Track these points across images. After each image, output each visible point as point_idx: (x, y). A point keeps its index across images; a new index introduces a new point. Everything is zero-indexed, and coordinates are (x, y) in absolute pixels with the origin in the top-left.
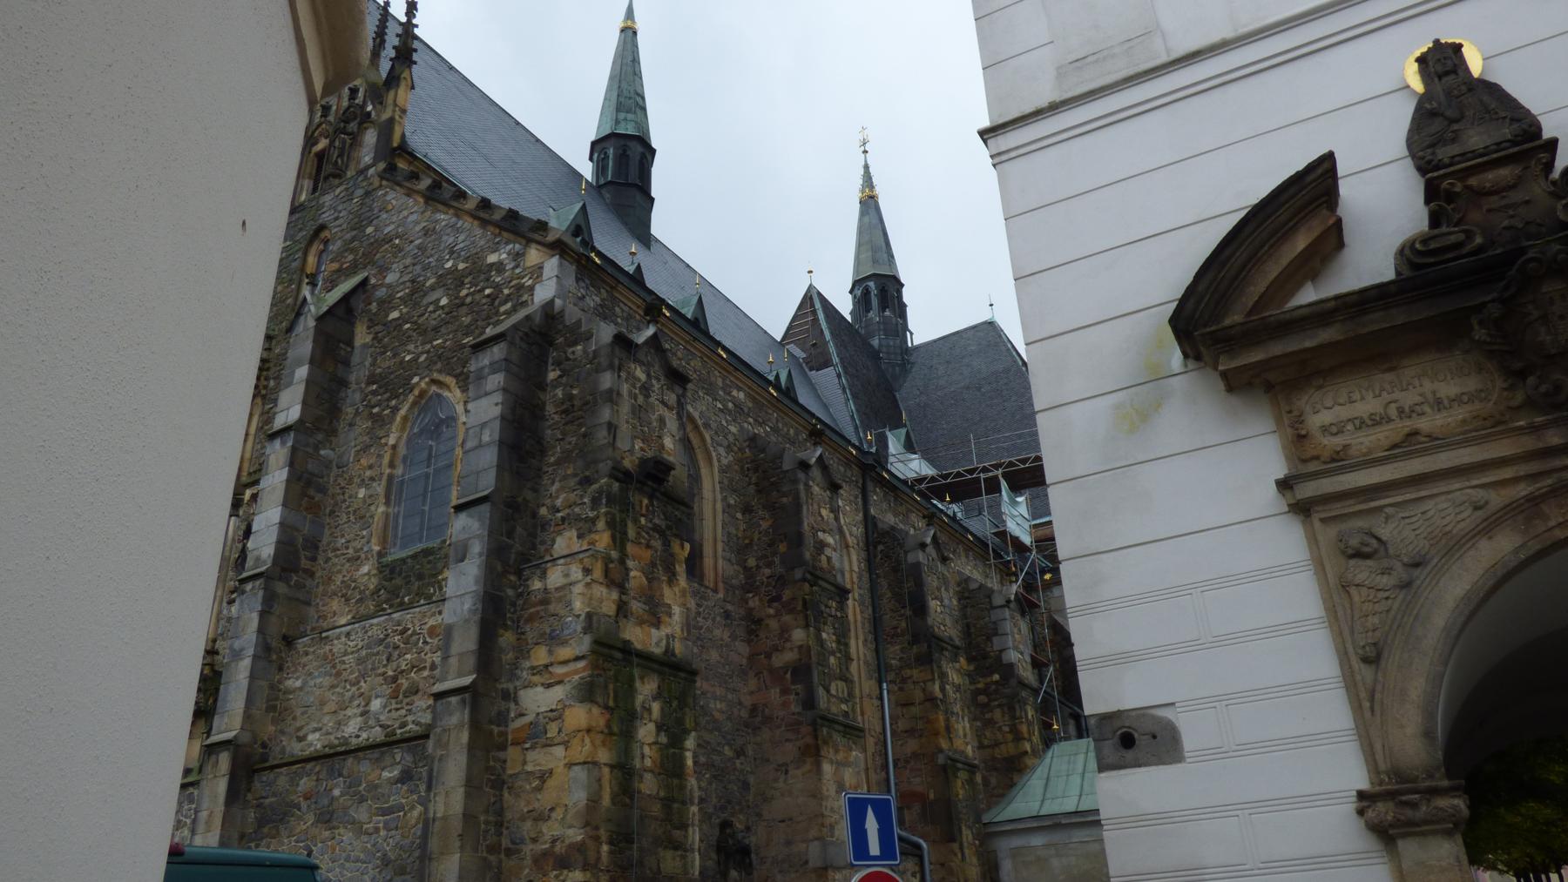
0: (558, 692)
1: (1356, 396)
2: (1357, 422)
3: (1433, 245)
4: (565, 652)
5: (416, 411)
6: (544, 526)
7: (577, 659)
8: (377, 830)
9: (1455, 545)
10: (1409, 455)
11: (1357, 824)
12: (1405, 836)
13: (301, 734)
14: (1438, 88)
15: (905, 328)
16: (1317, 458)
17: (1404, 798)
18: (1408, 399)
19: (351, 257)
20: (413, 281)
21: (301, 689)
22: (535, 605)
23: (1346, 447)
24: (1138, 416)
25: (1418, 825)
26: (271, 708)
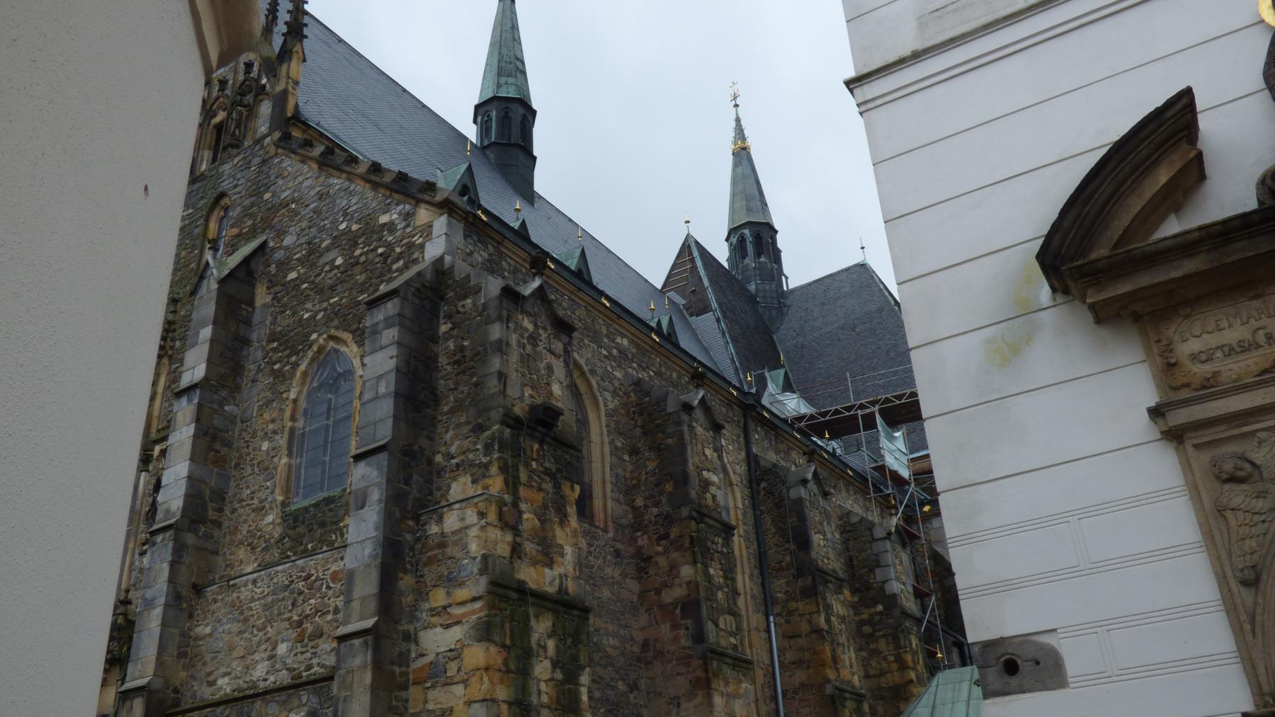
0: (457, 633)
1: (1224, 324)
2: (1226, 349)
4: (462, 594)
5: (315, 366)
7: (474, 599)
13: (211, 679)
15: (780, 272)
16: (1187, 385)
20: (309, 243)
21: (210, 635)
23: (1216, 374)
24: (1009, 351)
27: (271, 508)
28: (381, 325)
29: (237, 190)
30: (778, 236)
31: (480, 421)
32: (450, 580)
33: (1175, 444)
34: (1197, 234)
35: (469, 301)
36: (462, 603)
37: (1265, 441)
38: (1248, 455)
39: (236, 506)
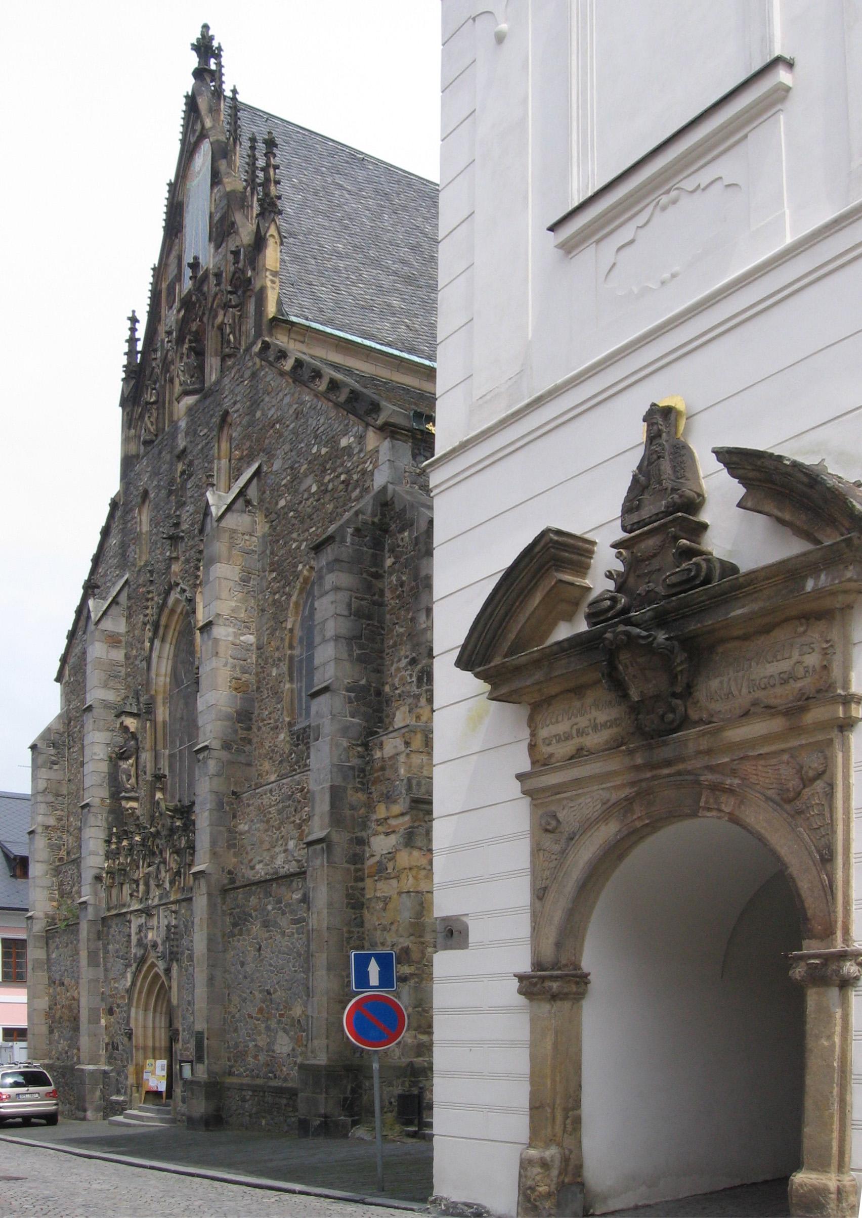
0: (393, 840)
4: (396, 809)
5: (304, 595)
6: (388, 702)
7: (402, 814)
8: (293, 934)
9: (588, 826)
13: (252, 864)
19: (248, 444)
20: (292, 468)
21: (248, 831)
22: (377, 771)
26: (231, 846)
27: (282, 728)
28: (324, 570)
29: (236, 407)
31: (414, 655)
32: (388, 798)
35: (406, 534)
36: (396, 817)
39: (261, 724)
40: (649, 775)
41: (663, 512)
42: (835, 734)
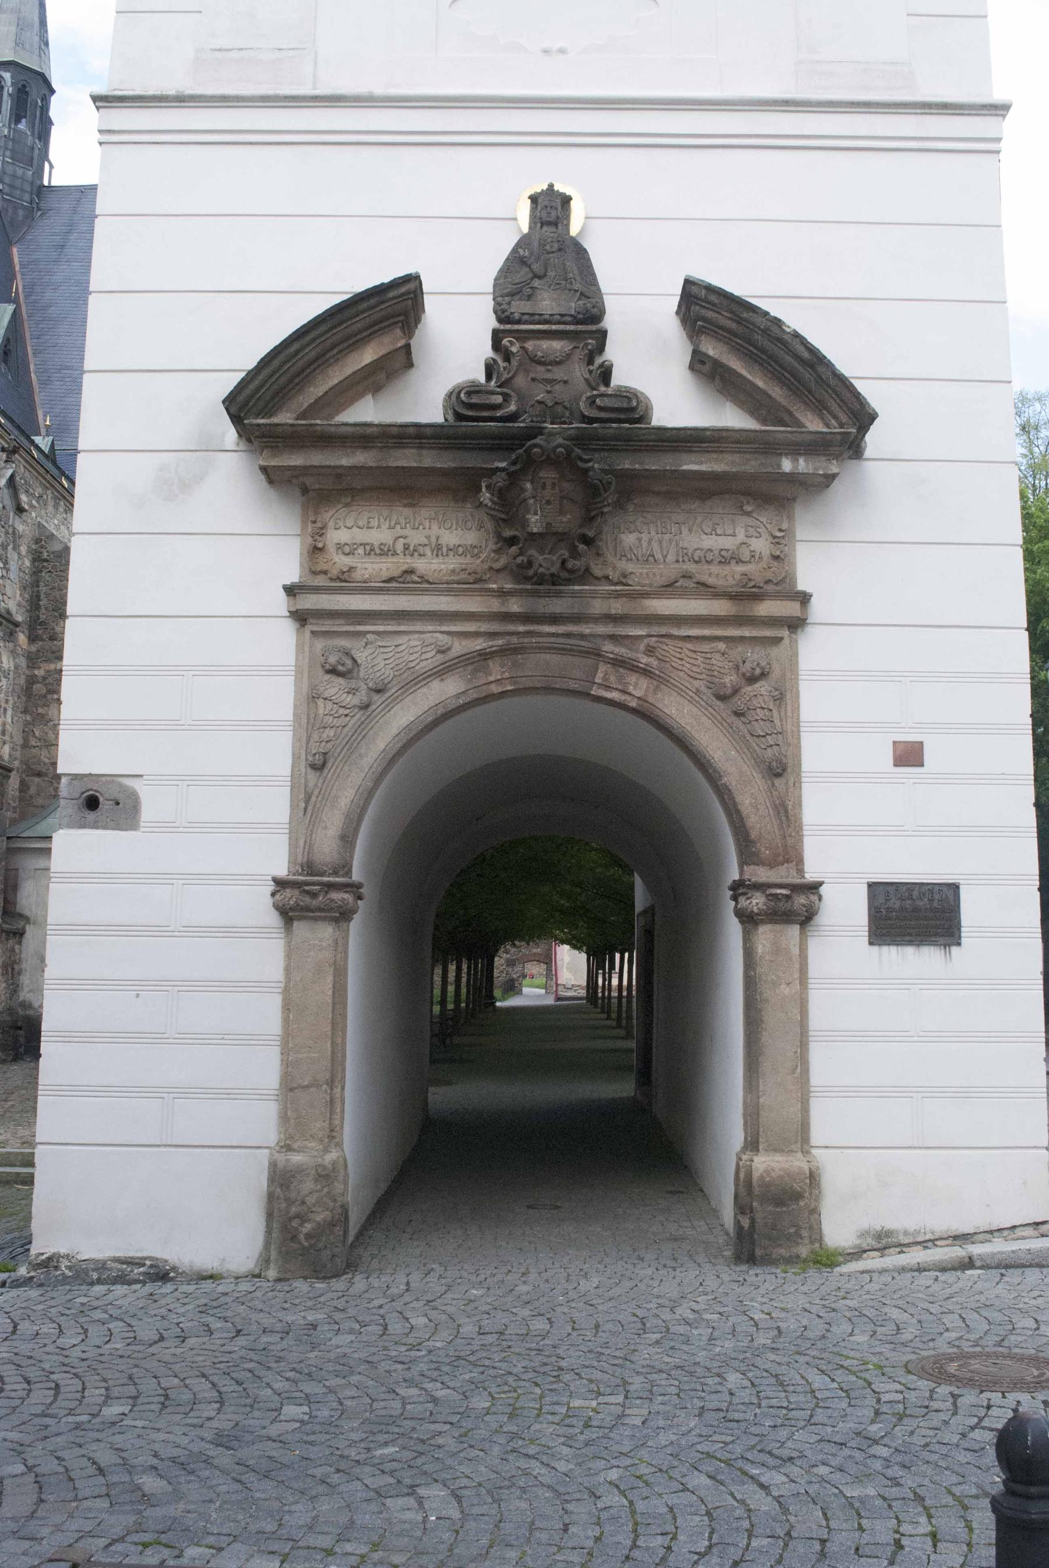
1: (374, 523)
2: (368, 548)
3: (474, 400)
10: (397, 591)
11: (268, 901)
12: (300, 918)
14: (536, 236)
15: (44, 155)
16: (325, 573)
17: (306, 888)
18: (416, 538)
23: (351, 569)
24: (177, 487)
25: (312, 911)
30: (54, 99)
33: (298, 626)
34: (375, 429)
37: (371, 643)
38: (353, 652)
40: (521, 628)
41: (571, 316)
42: (785, 633)
